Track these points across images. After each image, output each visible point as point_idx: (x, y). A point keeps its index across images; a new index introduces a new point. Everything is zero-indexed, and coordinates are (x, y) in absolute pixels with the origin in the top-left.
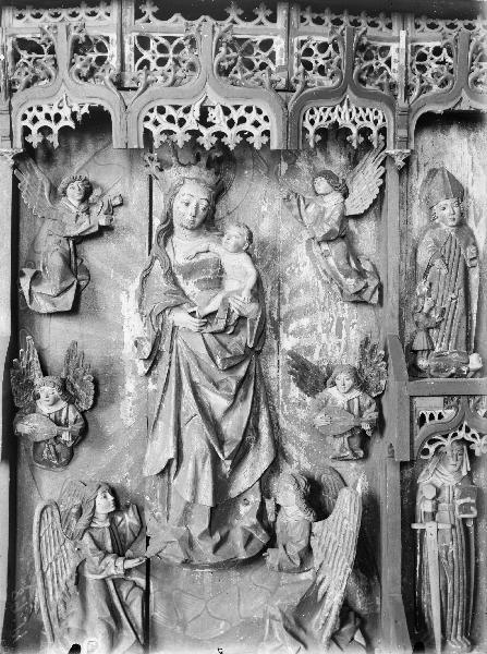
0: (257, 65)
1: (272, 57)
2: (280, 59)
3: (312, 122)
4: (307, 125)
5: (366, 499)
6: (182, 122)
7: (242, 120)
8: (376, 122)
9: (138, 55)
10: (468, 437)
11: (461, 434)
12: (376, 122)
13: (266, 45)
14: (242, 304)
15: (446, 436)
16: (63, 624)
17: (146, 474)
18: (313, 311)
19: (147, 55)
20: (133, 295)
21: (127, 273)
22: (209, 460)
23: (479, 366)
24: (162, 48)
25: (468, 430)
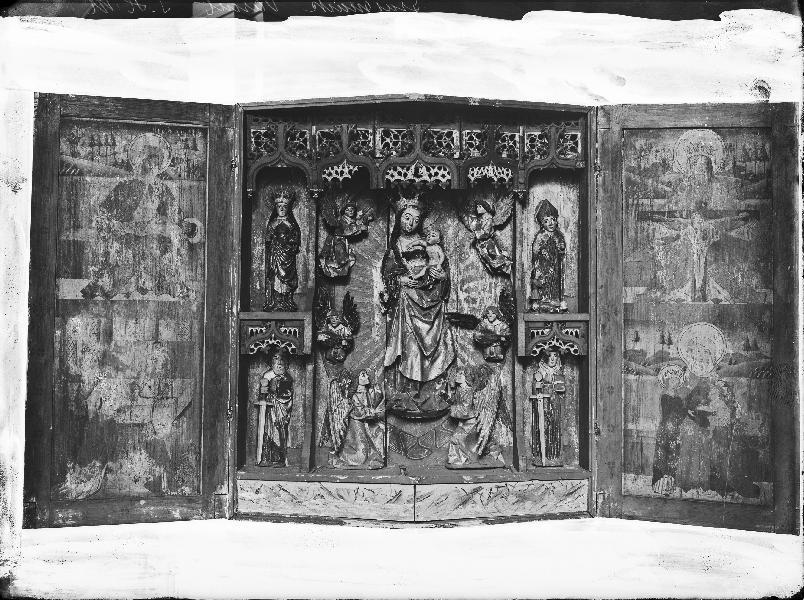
0: (444, 144)
1: (452, 140)
2: (457, 142)
3: (473, 175)
4: (470, 176)
5: (254, 207)
6: (405, 175)
7: (436, 174)
8: (507, 175)
9: (383, 140)
10: (558, 345)
11: (554, 343)
12: (507, 175)
13: (450, 134)
14: (437, 272)
15: (545, 344)
16: (742, 222)
17: (483, 361)
18: (476, 279)
19: (388, 140)
20: (379, 270)
21: (374, 255)
22: (419, 356)
23: (565, 308)
24: (396, 137)
25: (557, 341)
